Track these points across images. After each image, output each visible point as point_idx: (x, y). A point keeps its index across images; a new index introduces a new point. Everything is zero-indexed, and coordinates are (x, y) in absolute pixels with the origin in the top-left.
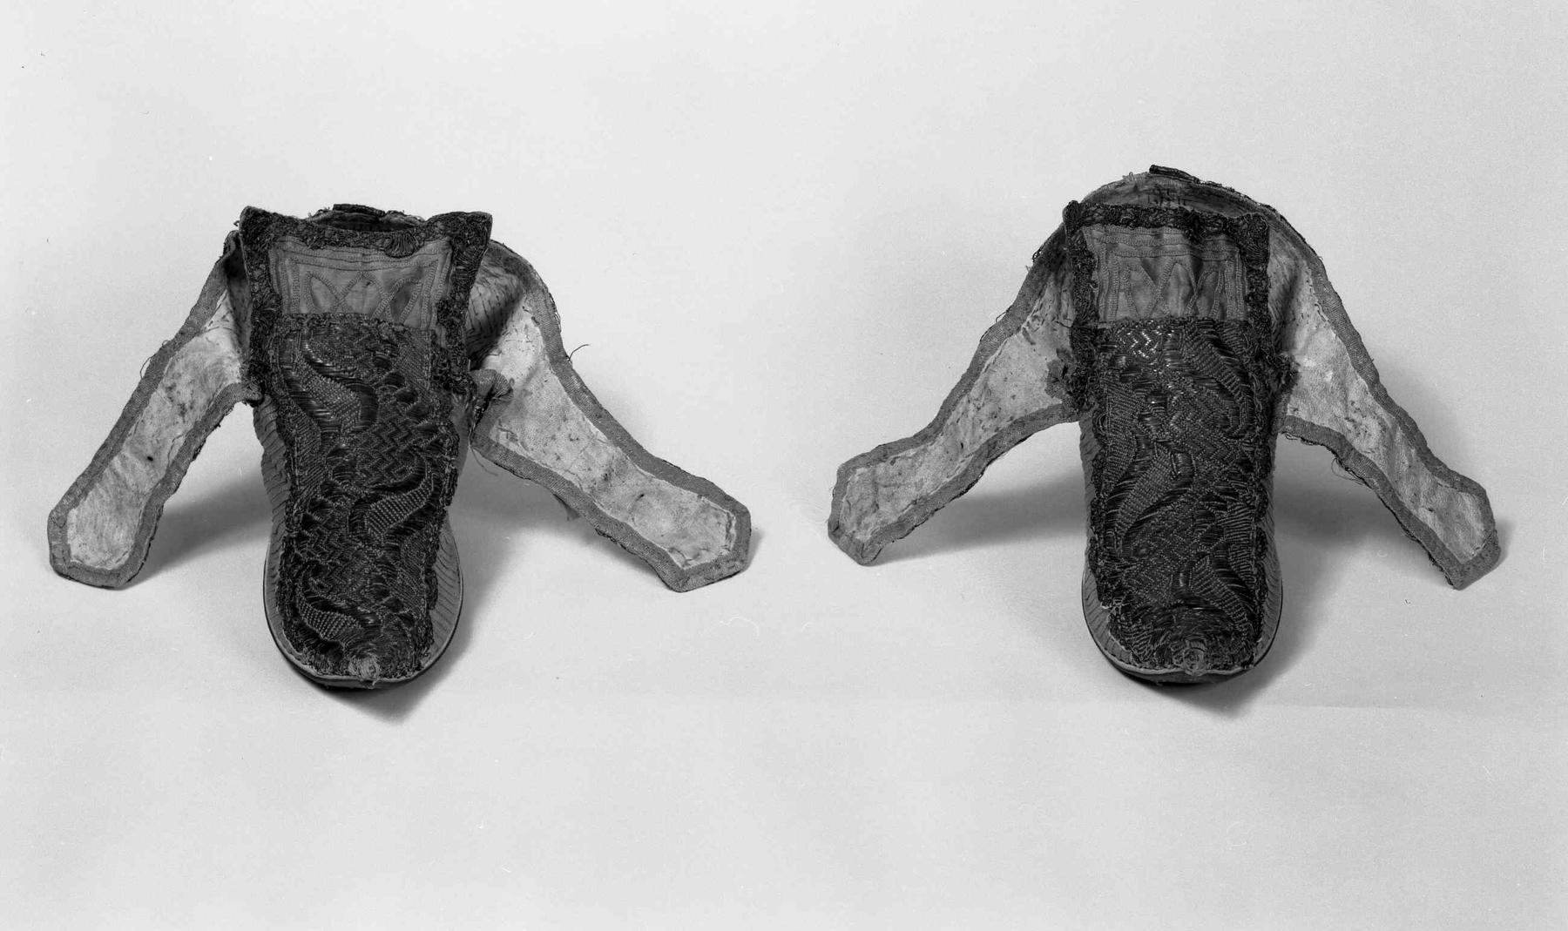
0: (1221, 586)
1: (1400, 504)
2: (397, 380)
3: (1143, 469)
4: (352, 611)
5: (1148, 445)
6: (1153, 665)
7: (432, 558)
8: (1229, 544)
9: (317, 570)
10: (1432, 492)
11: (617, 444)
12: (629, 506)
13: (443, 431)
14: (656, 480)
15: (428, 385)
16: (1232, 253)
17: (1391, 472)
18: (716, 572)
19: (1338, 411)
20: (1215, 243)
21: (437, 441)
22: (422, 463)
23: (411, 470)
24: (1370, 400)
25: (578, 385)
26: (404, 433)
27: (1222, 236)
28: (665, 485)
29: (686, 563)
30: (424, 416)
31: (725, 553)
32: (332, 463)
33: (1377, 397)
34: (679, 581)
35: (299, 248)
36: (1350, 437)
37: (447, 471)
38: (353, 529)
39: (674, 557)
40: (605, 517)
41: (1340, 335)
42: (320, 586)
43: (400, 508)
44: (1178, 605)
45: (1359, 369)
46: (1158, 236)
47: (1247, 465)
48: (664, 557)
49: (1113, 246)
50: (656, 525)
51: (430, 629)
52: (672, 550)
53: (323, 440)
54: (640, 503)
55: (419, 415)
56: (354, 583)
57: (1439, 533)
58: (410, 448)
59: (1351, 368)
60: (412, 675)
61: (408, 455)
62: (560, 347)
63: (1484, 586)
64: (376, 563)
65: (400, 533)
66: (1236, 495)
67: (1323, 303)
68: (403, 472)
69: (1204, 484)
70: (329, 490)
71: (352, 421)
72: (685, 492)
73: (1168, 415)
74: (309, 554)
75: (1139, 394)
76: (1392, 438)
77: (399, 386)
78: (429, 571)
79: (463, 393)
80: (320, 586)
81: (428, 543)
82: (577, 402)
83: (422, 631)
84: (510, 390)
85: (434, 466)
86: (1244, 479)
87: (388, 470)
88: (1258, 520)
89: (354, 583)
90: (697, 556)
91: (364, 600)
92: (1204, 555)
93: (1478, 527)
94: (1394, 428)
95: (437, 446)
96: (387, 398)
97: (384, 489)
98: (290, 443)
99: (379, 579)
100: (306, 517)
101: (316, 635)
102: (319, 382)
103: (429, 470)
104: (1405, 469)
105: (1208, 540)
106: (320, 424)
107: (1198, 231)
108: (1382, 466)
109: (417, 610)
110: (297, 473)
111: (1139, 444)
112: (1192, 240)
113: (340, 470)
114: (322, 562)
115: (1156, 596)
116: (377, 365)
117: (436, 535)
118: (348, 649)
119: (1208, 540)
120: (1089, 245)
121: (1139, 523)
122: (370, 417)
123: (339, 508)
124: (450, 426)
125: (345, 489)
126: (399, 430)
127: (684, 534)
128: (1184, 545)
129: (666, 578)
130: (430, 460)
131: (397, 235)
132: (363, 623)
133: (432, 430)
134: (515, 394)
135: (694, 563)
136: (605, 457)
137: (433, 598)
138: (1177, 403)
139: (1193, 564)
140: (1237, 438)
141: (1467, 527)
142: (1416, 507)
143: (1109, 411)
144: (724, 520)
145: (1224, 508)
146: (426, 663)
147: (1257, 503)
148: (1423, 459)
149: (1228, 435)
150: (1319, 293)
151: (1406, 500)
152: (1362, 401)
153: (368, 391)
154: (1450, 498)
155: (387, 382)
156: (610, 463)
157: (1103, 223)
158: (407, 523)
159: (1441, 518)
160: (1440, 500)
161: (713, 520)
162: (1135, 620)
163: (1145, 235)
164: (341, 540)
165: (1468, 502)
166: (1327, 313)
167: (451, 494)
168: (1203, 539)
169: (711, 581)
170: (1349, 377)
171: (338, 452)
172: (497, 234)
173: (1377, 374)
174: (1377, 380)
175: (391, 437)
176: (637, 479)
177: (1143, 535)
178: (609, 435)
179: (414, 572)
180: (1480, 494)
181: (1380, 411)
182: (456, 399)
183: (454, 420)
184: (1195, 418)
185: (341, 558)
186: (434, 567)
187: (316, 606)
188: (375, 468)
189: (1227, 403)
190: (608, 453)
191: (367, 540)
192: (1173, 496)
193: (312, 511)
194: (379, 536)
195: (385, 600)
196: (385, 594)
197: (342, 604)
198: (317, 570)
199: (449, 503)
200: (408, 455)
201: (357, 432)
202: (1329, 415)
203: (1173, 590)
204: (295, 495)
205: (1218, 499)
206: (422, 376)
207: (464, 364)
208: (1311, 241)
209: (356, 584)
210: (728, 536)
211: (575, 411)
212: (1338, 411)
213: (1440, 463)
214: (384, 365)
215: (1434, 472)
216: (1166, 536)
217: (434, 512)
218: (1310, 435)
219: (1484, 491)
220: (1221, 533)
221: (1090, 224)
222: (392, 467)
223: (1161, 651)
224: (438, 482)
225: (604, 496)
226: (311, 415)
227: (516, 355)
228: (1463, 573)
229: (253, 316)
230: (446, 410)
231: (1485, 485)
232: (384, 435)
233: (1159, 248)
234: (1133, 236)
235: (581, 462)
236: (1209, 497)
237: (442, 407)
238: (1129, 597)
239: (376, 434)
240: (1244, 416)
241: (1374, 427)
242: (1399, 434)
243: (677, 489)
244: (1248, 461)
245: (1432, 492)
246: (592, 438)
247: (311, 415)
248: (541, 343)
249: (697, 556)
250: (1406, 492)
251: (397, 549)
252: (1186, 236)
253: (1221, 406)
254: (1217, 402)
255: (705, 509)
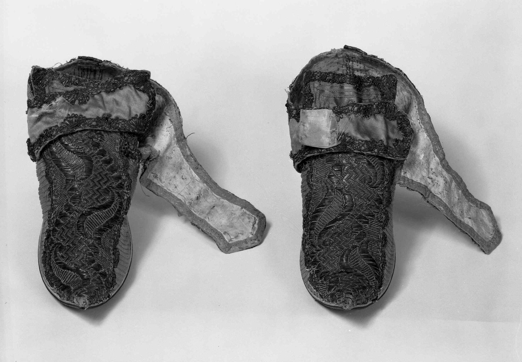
0: (363, 262)
1: (455, 217)
2: (103, 153)
3: (330, 202)
4: (77, 271)
5: (332, 190)
6: (329, 301)
7: (116, 242)
8: (369, 241)
9: (61, 248)
10: (469, 210)
11: (206, 182)
12: (207, 212)
13: (124, 178)
14: (222, 200)
15: (117, 155)
16: (377, 95)
17: (450, 202)
18: (244, 245)
19: (424, 174)
20: (368, 91)
21: (121, 183)
22: (113, 195)
23: (108, 198)
24: (440, 168)
25: (189, 153)
26: (106, 180)
27: (372, 87)
28: (226, 202)
29: (231, 240)
30: (116, 171)
31: (251, 236)
32: (70, 195)
33: (443, 166)
34: (227, 248)
35: (59, 86)
36: (429, 187)
37: (125, 198)
38: (79, 228)
39: (226, 237)
40: (196, 217)
41: (429, 136)
42: (62, 257)
43: (100, 218)
44: (342, 272)
45: (436, 153)
46: (342, 87)
47: (380, 202)
48: (221, 236)
49: (322, 91)
50: (218, 221)
51: (114, 277)
52: (225, 233)
53: (67, 183)
54: (212, 210)
55: (113, 170)
56: (78, 256)
57: (475, 228)
58: (108, 187)
59: (432, 152)
60: (105, 300)
61: (107, 191)
62: (182, 134)
63: (497, 252)
64: (89, 246)
65: (101, 231)
66: (373, 216)
67: (422, 119)
68: (104, 199)
69: (358, 210)
70: (68, 208)
71: (81, 173)
72: (235, 206)
73: (343, 176)
74: (57, 239)
75: (330, 165)
76: (450, 186)
77: (104, 156)
78: (115, 249)
79: (135, 159)
80: (62, 257)
81: (115, 234)
82: (187, 161)
83: (110, 279)
84: (158, 156)
85: (119, 196)
86: (378, 208)
87: (97, 199)
88: (383, 228)
89: (78, 256)
90: (236, 237)
91: (83, 265)
92: (356, 247)
93: (490, 225)
94: (451, 182)
95: (121, 186)
96: (98, 162)
97: (94, 208)
98: (51, 183)
99: (90, 254)
100: (57, 220)
101: (60, 281)
102: (66, 153)
103: (117, 198)
104: (456, 200)
105: (358, 239)
106: (66, 175)
107: (360, 85)
108: (445, 200)
109: (108, 269)
110: (54, 198)
111: (328, 190)
112: (357, 89)
113: (74, 198)
114: (63, 244)
115: (332, 266)
116: (93, 146)
117: (119, 231)
118: (75, 290)
119: (358, 239)
120: (312, 91)
121: (326, 229)
122: (89, 171)
123: (72, 217)
124: (128, 175)
125: (75, 208)
126: (103, 178)
127: (232, 226)
128: (346, 241)
129: (220, 246)
130: (118, 193)
131: (107, 78)
132: (82, 277)
133: (119, 178)
134: (161, 158)
135: (235, 240)
136: (198, 188)
137: (116, 262)
138: (347, 170)
139: (350, 251)
140: (375, 187)
141: (485, 225)
142: (463, 218)
143: (314, 172)
144: (252, 220)
145: (367, 223)
146: (112, 294)
147: (384, 219)
148: (465, 195)
149: (371, 186)
150: (420, 114)
151: (458, 216)
152: (436, 169)
153: (88, 159)
154: (477, 212)
155: (98, 154)
156: (200, 191)
157: (319, 80)
158: (104, 226)
159: (474, 222)
160: (472, 213)
161: (247, 220)
162: (321, 278)
163: (336, 86)
164: (72, 234)
165: (484, 213)
166: (423, 124)
167: (127, 209)
168: (357, 238)
169: (242, 249)
170: (431, 156)
171: (73, 189)
172: (152, 77)
173: (444, 155)
174: (444, 158)
175: (99, 182)
176: (213, 199)
177: (328, 235)
178: (201, 177)
179: (107, 250)
180: (488, 209)
181: (445, 173)
182: (131, 162)
183: (130, 172)
184: (355, 178)
185: (72, 243)
186: (118, 246)
187: (60, 266)
188: (90, 198)
189: (371, 171)
190: (200, 186)
191: (85, 235)
192: (343, 216)
193: (60, 218)
194: (91, 233)
195: (93, 265)
196: (93, 261)
197: (73, 266)
198: (61, 248)
199: (126, 213)
200: (107, 191)
201: (82, 179)
202: (420, 176)
203: (340, 264)
204: (52, 209)
205: (365, 218)
206: (115, 151)
207: (135, 144)
208: (419, 87)
209: (78, 257)
210: (253, 228)
211: (186, 165)
212: (424, 174)
213: (472, 196)
214: (97, 145)
215: (469, 200)
216: (338, 236)
217: (119, 218)
218: (411, 185)
219: (490, 208)
220: (365, 236)
221: (313, 80)
222: (99, 197)
223: (332, 295)
224: (121, 204)
225: (196, 207)
226: (62, 170)
227: (164, 139)
228: (489, 246)
229: (75, 116)
230: (126, 166)
231: (490, 205)
232: (95, 181)
233: (342, 93)
234: (332, 87)
235: (186, 190)
236: (360, 217)
237: (124, 166)
238: (319, 266)
239: (92, 181)
240: (379, 177)
241: (441, 181)
242: (454, 184)
243: (231, 204)
244: (380, 199)
245: (469, 210)
246: (192, 178)
247: (62, 170)
248: (174, 133)
249: (236, 237)
250: (457, 211)
251: (99, 239)
252: (355, 88)
253: (368, 172)
254: (366, 170)
255: (244, 214)
